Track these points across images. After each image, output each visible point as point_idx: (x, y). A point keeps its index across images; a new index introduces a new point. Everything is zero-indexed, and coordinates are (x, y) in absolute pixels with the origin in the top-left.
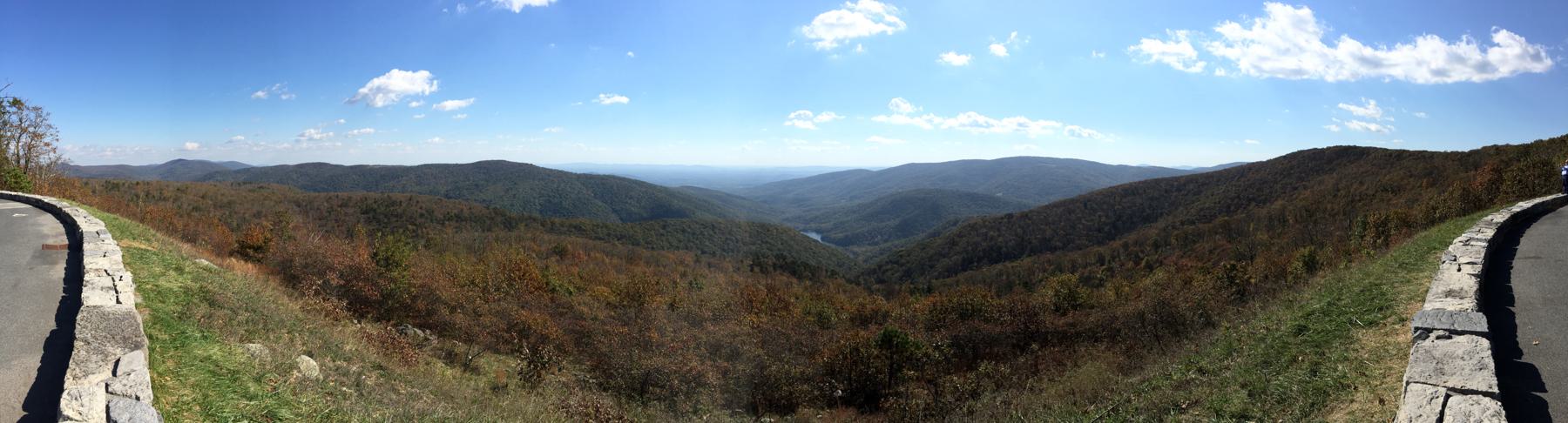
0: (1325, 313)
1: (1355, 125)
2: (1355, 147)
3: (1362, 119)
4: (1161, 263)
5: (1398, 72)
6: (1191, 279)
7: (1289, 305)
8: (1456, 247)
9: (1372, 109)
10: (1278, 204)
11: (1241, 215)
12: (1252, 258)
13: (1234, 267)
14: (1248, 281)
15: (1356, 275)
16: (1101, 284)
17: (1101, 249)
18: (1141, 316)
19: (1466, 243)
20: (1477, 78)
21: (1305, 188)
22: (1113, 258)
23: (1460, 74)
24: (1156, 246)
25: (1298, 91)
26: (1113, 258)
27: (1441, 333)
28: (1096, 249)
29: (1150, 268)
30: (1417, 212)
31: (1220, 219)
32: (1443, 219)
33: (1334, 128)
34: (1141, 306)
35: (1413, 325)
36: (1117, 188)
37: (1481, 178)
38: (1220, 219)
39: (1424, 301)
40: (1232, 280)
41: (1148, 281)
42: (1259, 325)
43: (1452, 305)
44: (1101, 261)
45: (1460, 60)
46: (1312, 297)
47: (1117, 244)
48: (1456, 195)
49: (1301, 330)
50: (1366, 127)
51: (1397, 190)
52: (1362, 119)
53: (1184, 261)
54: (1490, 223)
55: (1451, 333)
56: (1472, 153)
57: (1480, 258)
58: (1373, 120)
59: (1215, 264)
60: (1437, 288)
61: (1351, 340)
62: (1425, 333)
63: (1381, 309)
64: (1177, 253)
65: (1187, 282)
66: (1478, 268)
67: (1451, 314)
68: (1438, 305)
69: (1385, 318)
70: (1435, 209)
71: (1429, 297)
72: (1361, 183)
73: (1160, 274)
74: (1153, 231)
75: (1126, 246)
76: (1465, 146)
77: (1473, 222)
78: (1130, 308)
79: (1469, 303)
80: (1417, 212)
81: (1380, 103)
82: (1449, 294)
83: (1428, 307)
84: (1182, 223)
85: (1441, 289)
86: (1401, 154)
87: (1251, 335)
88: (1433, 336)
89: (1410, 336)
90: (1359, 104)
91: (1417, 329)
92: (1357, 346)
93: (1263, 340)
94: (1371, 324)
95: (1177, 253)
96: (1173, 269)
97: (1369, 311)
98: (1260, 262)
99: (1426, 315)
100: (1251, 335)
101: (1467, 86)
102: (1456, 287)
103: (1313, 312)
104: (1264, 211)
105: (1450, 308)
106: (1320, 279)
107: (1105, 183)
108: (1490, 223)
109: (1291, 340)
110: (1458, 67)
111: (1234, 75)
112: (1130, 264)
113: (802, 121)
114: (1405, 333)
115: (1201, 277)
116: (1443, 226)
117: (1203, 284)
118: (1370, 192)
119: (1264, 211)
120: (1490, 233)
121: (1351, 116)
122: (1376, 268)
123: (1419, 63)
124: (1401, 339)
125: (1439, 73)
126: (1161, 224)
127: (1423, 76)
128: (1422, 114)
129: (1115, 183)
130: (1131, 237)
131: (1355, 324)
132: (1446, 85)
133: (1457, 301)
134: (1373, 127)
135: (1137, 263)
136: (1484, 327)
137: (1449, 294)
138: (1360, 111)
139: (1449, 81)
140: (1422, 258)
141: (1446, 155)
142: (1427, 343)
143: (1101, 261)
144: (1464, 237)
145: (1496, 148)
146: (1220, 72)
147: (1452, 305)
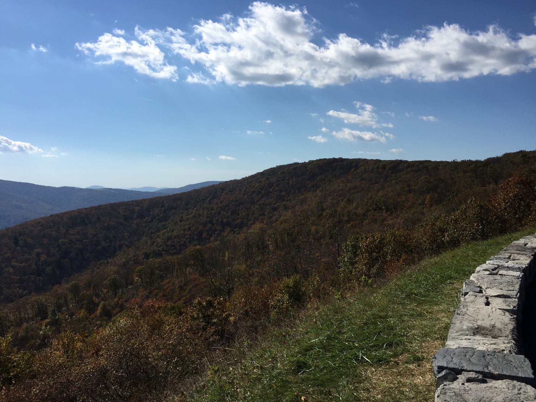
0: (325, 348)
1: (346, 134)
2: (341, 160)
3: (353, 126)
4: (122, 308)
5: (400, 70)
6: (161, 323)
7: (283, 340)
8: (479, 275)
9: (367, 114)
10: (256, 228)
11: (215, 243)
12: (229, 292)
13: (210, 304)
14: (226, 318)
15: (356, 304)
16: (45, 343)
17: (42, 298)
18: (103, 373)
19: (494, 272)
20: (506, 70)
21: (286, 208)
22: (59, 307)
23: (482, 66)
24: (115, 286)
25: (281, 99)
26: (59, 307)
27: (472, 375)
28: (34, 298)
29: (108, 315)
30: (420, 235)
31: (191, 249)
32: (455, 243)
33: (320, 139)
34: (103, 361)
35: (436, 364)
36: (61, 216)
37: (502, 197)
38: (191, 249)
39: (444, 338)
40: (207, 319)
41: (107, 331)
42: (251, 364)
43: (482, 344)
44: (42, 313)
45: (484, 50)
46: (309, 327)
47: (64, 288)
48: (471, 213)
49: (300, 366)
50: (359, 136)
51: (392, 209)
52: (353, 126)
53: (149, 302)
54: (523, 249)
55: (485, 377)
56: (490, 161)
57: (514, 290)
58: (369, 129)
59: (188, 302)
60: (461, 323)
61: (358, 379)
62: (453, 373)
63: (390, 345)
64: (142, 292)
65: (157, 327)
66: (513, 303)
67: (483, 355)
68: (465, 343)
69: (396, 355)
70: (442, 231)
71: (452, 333)
72: (350, 201)
73: (123, 322)
74: (111, 269)
75: (75, 290)
76: (481, 154)
77: (498, 248)
78: (89, 366)
79: (505, 344)
80: (420, 235)
81: (377, 110)
82: (477, 331)
83: (451, 344)
84: (147, 256)
85: (466, 325)
86: (397, 166)
87: (245, 376)
88: (462, 378)
89: (429, 377)
90: (353, 110)
91: (441, 369)
92: (367, 385)
93: (258, 380)
94: (379, 362)
95: (142, 292)
96: (137, 312)
97: (377, 347)
98: (239, 298)
99: (448, 351)
100: (245, 376)
101: (490, 81)
102: (486, 323)
103: (312, 347)
104: (241, 237)
105: (481, 348)
106: (314, 310)
107: (45, 210)
108: (523, 249)
109: (291, 378)
110: (478, 58)
111: (207, 82)
112: (82, 313)
113: (370, 76)
114: (423, 374)
115: (172, 319)
116: (458, 251)
117: (174, 328)
118: (360, 211)
119: (241, 237)
120: (525, 261)
121: (340, 124)
122: (378, 297)
123: (427, 57)
124: (418, 380)
125: (450, 67)
126: (120, 259)
127: (433, 73)
128: (431, 118)
129: (58, 210)
130: (82, 278)
131: (362, 361)
132: (463, 81)
133: (488, 340)
134: (367, 136)
135: (91, 310)
136: (529, 373)
137: (477, 331)
138: (353, 118)
139: (467, 75)
140: (435, 288)
141: (455, 165)
142: (456, 385)
143: (42, 313)
144: (489, 264)
145: (523, 154)
146: (193, 79)
147: (482, 344)
